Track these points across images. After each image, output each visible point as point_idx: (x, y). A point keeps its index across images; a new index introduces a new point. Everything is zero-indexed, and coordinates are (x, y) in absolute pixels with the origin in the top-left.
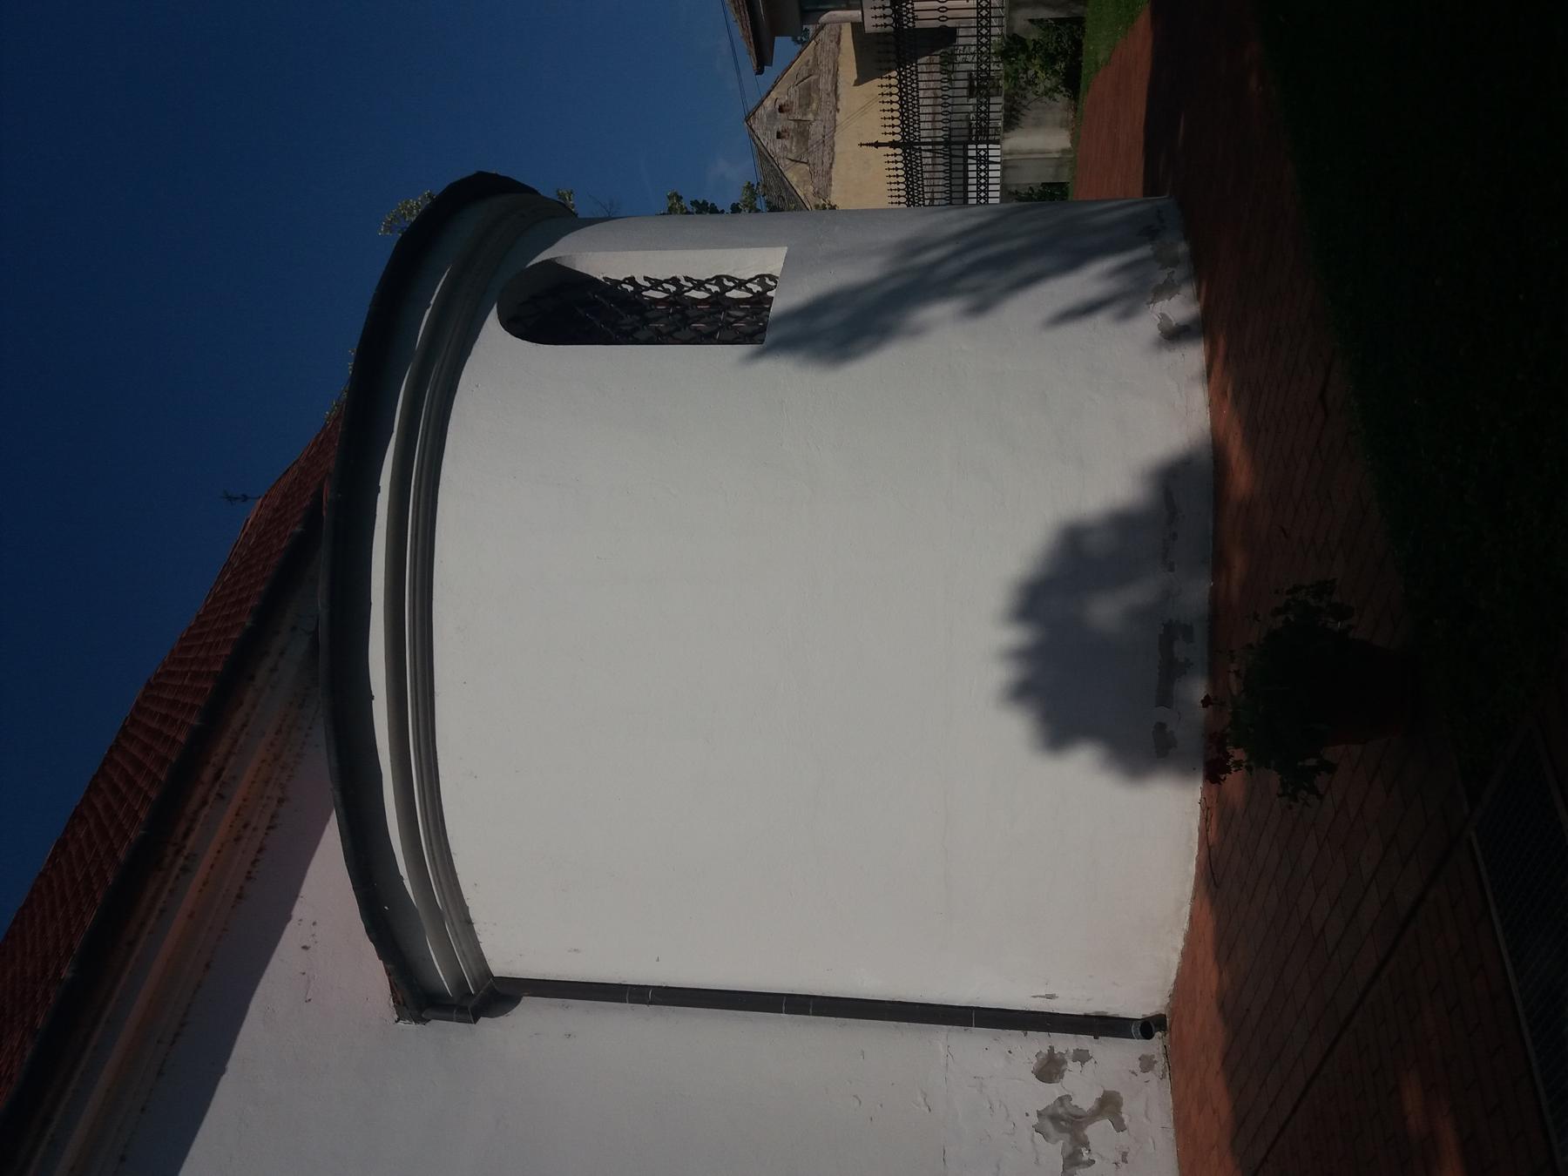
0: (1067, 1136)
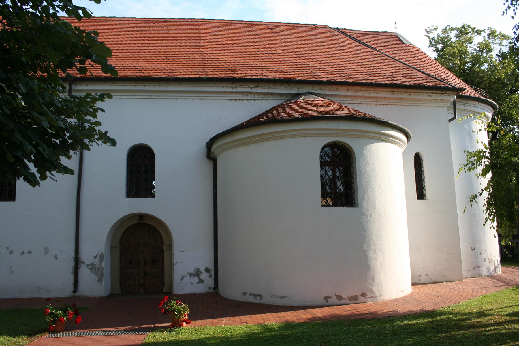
0: (195, 273)
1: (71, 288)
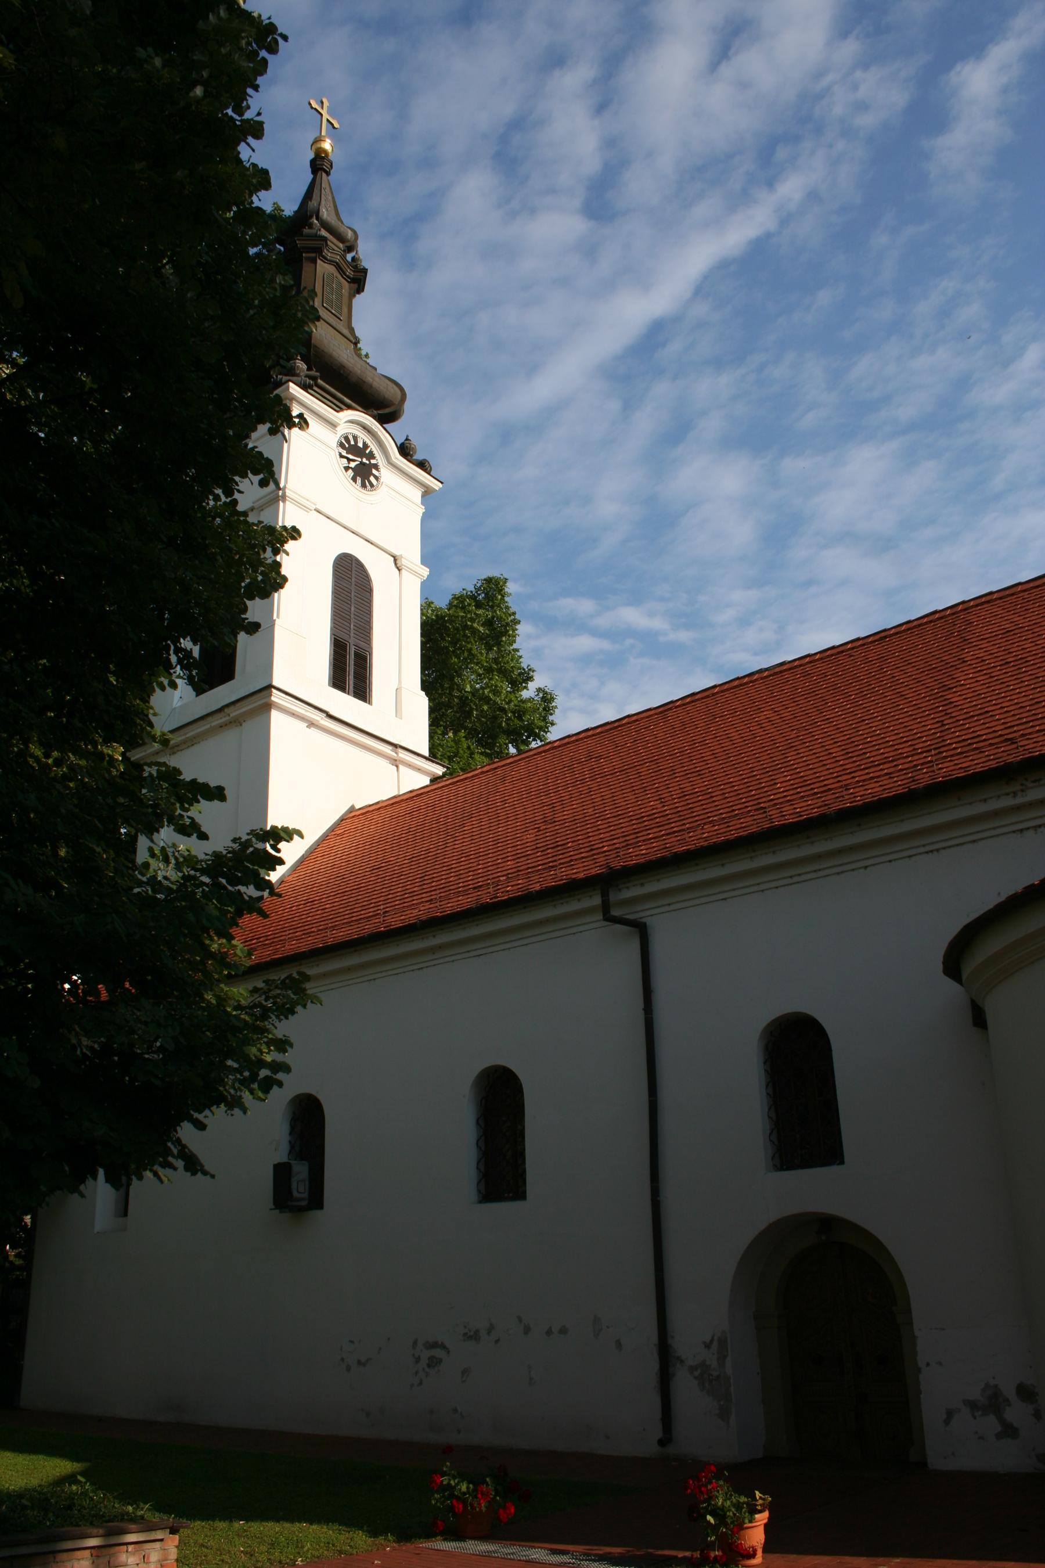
1: (658, 1433)
